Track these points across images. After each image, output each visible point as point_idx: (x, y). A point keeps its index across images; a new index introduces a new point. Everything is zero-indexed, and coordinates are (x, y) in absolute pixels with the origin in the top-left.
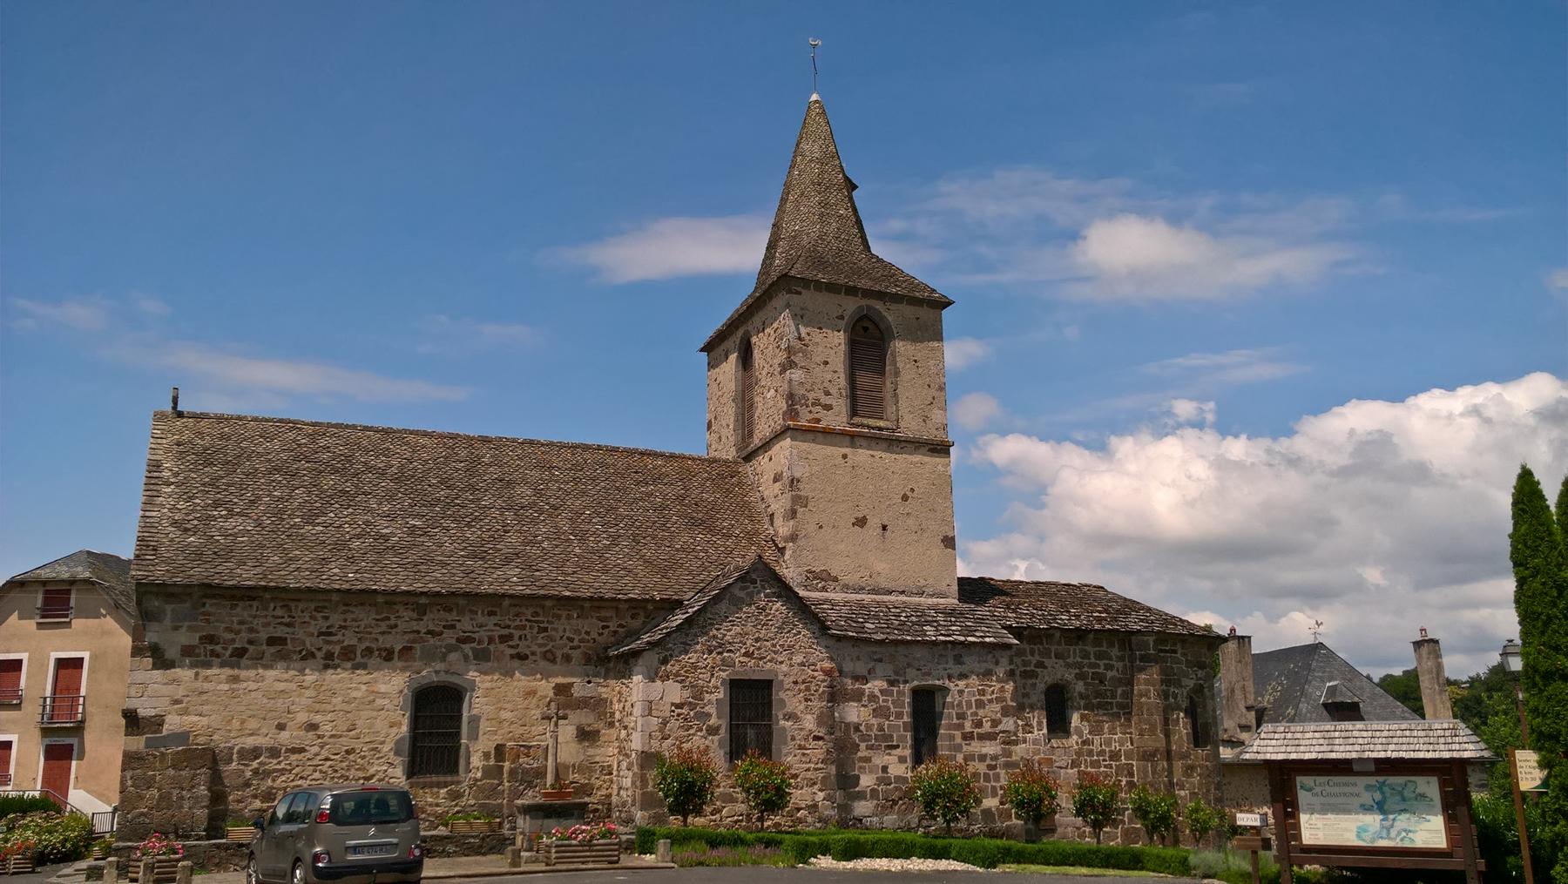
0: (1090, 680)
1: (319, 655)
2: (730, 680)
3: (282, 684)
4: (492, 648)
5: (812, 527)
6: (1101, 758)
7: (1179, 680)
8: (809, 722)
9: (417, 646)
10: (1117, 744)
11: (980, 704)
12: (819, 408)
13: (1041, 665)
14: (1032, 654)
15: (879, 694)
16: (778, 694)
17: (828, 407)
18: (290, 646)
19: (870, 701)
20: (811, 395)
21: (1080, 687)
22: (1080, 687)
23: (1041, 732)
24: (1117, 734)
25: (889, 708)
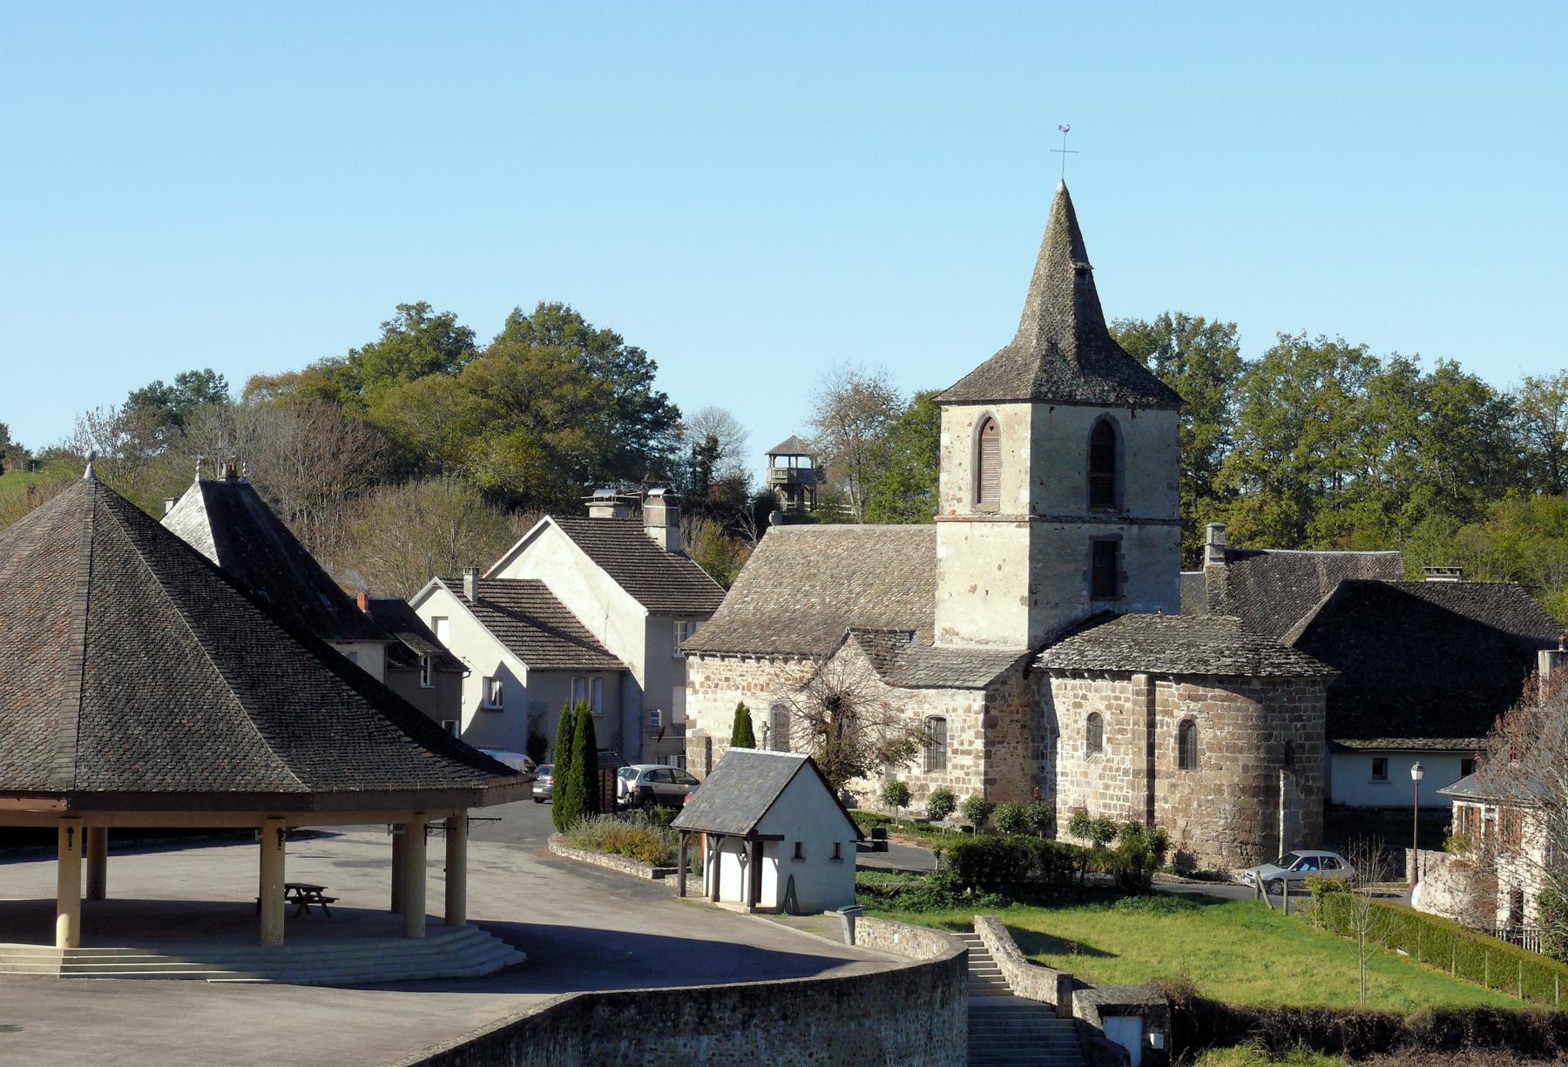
3: (1086, 526)
5: (946, 596)
11: (963, 730)
13: (1084, 697)
17: (960, 500)
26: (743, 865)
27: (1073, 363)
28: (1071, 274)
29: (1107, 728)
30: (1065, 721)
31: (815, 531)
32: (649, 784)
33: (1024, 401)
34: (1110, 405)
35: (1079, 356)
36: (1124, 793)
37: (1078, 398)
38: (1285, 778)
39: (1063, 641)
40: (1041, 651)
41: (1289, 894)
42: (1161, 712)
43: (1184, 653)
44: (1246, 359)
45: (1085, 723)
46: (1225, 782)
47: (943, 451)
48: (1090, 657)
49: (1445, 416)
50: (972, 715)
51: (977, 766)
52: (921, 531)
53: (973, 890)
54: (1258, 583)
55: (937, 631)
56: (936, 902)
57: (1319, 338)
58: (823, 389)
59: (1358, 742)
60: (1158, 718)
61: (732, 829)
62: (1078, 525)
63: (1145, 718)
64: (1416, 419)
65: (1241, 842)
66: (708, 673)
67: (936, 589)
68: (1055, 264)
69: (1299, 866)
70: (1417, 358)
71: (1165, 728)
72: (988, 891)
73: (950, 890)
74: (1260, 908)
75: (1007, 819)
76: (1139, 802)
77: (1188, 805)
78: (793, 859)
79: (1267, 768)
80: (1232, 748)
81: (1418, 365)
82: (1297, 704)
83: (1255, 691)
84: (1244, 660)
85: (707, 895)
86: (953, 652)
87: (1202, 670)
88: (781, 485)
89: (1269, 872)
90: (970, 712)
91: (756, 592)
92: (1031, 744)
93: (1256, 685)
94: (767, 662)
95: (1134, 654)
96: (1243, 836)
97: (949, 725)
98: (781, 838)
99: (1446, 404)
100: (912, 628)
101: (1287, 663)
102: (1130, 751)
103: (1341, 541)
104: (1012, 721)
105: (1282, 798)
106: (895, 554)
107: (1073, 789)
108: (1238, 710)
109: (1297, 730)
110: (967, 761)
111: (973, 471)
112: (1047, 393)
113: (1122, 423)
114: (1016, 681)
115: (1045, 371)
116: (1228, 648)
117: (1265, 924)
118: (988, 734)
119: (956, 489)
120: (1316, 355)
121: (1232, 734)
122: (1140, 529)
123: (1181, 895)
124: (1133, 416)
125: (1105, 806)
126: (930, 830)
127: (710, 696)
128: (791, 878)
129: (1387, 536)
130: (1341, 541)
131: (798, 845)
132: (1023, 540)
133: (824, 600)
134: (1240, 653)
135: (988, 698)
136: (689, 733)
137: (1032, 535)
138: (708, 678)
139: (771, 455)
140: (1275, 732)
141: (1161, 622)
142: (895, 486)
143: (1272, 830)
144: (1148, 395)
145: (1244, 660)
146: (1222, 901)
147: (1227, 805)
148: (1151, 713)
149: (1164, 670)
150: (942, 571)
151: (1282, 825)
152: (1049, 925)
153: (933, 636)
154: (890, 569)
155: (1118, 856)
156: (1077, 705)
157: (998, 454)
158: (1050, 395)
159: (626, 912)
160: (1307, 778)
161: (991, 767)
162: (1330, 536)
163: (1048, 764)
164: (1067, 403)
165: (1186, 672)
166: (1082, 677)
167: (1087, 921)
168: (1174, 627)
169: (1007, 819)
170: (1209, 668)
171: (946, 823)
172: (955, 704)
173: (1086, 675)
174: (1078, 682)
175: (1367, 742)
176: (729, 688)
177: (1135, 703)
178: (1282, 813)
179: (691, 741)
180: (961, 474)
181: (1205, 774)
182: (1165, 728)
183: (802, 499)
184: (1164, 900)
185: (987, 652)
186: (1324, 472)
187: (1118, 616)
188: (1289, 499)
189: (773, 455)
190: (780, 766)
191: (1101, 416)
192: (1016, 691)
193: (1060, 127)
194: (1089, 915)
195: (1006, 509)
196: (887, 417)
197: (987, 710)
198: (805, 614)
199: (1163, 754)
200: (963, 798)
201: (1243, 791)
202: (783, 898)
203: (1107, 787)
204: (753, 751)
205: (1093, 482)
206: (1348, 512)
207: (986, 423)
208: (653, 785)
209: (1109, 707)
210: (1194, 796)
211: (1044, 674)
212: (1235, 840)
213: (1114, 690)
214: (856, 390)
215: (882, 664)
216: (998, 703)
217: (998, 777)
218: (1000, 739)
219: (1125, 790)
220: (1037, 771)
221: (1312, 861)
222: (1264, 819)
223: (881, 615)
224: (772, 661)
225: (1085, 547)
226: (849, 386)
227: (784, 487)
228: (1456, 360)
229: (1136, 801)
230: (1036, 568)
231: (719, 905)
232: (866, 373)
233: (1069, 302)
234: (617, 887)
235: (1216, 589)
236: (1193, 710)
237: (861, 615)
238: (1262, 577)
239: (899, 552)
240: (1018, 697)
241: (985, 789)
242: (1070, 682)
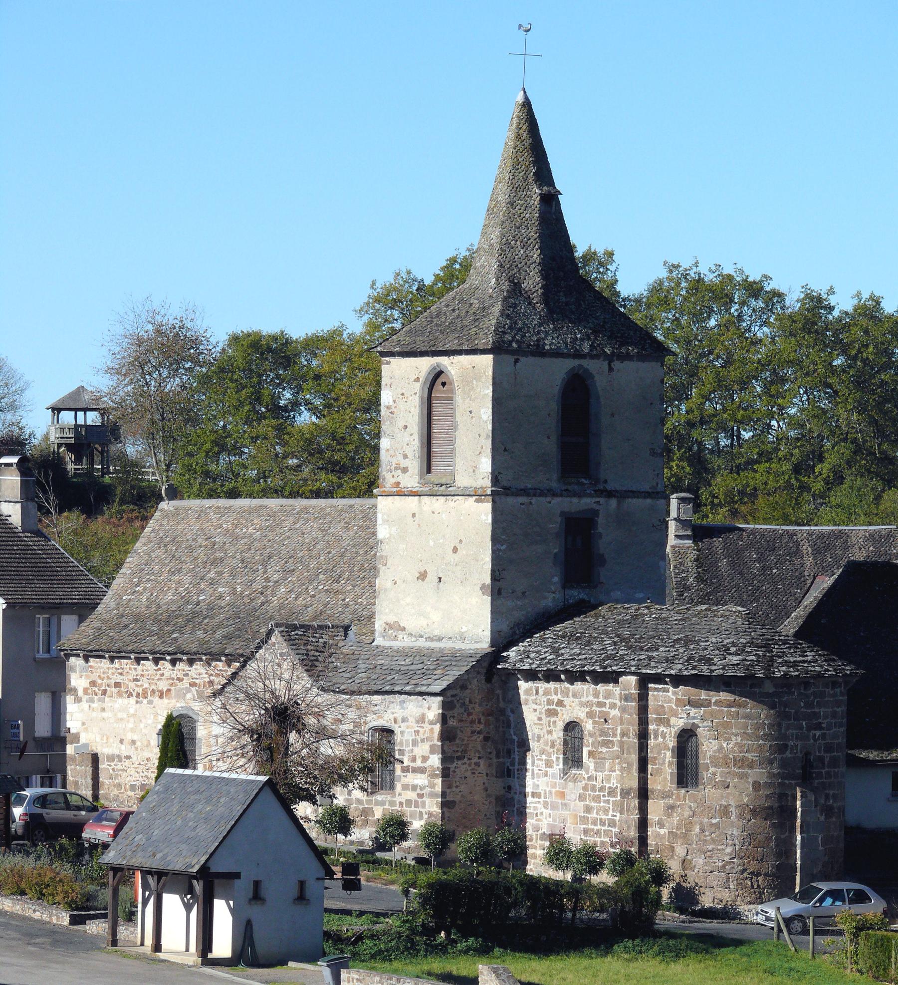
1: (134, 694)
5: (389, 584)
6: (602, 794)
7: (668, 720)
10: (615, 781)
11: (415, 743)
13: (560, 703)
17: (405, 470)
18: (122, 689)
23: (558, 767)
26: (188, 908)
27: (540, 307)
28: (536, 201)
29: (588, 740)
30: (536, 731)
31: (218, 507)
32: (39, 811)
33: (484, 352)
34: (583, 356)
35: (547, 297)
36: (610, 817)
37: (547, 347)
38: (802, 797)
39: (532, 637)
40: (507, 648)
41: (816, 933)
42: (656, 719)
43: (681, 650)
44: (624, 293)
45: (561, 734)
46: (732, 803)
47: (383, 411)
48: (567, 656)
49: (865, 361)
50: (426, 725)
51: (432, 786)
52: (351, 506)
53: (448, 934)
54: (732, 565)
55: (379, 626)
56: (407, 949)
57: (713, 268)
58: (119, 330)
59: (875, 753)
60: (652, 727)
61: (178, 865)
62: (548, 499)
63: (636, 727)
64: (830, 364)
65: (752, 873)
66: (94, 677)
67: (376, 577)
68: (517, 189)
69: (822, 900)
70: (831, 291)
71: (660, 739)
72: (465, 936)
73: (421, 934)
74: (782, 951)
75: (474, 850)
76: (629, 827)
77: (689, 831)
78: (250, 900)
79: (781, 785)
80: (740, 762)
81: (833, 300)
82: (817, 710)
83: (768, 695)
84: (754, 658)
85: (142, 944)
86: (398, 651)
87: (705, 670)
88: (67, 445)
89: (789, 907)
90: (424, 722)
91: (149, 580)
92: (495, 760)
93: (769, 688)
94: (167, 665)
95: (621, 652)
96: (754, 866)
97: (398, 738)
98: (237, 875)
99: (867, 346)
100: (347, 622)
101: (804, 662)
102: (617, 767)
103: (744, 509)
104: (473, 732)
105: (799, 821)
106: (320, 534)
107: (546, 812)
108: (747, 717)
109: (815, 740)
110: (421, 780)
111: (421, 436)
112: (511, 342)
113: (597, 378)
114: (477, 684)
115: (508, 316)
116: (734, 644)
117: (791, 969)
118: (445, 748)
119: (400, 458)
120: (711, 289)
121: (740, 746)
122: (619, 503)
123: (690, 937)
124: (611, 369)
125: (586, 832)
126: (377, 862)
127: (95, 705)
128: (249, 924)
129: (797, 504)
130: (744, 509)
131: (257, 884)
132: (483, 517)
133: (235, 589)
134: (748, 649)
135: (446, 706)
136: (70, 749)
137: (494, 510)
138: (93, 683)
139: (53, 409)
140: (791, 743)
141: (650, 614)
142: (208, 446)
143: (787, 857)
144: (628, 344)
145: (754, 658)
146: (737, 943)
147: (735, 830)
148: (643, 721)
149: (659, 671)
150: (383, 554)
151: (799, 852)
152: (543, 974)
153: (373, 632)
154: (314, 552)
155: (616, 892)
156: (551, 713)
157: (453, 415)
158: (515, 345)
159: (54, 965)
160: (827, 797)
161: (450, 787)
162: (729, 503)
163: (515, 783)
164: (533, 354)
165: (685, 673)
166: (558, 679)
167: (585, 968)
168: (665, 619)
169: (474, 850)
170: (713, 668)
171: (395, 854)
172: (406, 713)
173: (563, 677)
174: (552, 685)
175: (886, 753)
176: (120, 695)
177: (623, 710)
178: (799, 838)
179: (73, 759)
180: (407, 439)
181: (709, 793)
182: (660, 739)
183: (91, 462)
184: (671, 942)
185: (441, 650)
186: (723, 427)
187: (595, 607)
188: (680, 460)
189: (56, 410)
190: (233, 790)
191: (573, 368)
192: (478, 698)
193: (520, 26)
194: (585, 962)
195: (463, 480)
196: (196, 363)
197: (444, 719)
198: (211, 607)
199: (658, 769)
200: (417, 825)
201: (754, 812)
202: (239, 949)
203: (588, 809)
204: (188, 772)
205: (565, 447)
206: (751, 474)
207: (437, 377)
208: (44, 811)
209: (590, 715)
210: (695, 819)
211: (511, 676)
212: (744, 870)
213: (596, 695)
214: (159, 332)
215: (310, 665)
216: (458, 710)
217: (458, 798)
218: (459, 754)
219: (611, 813)
220: (503, 792)
221: (836, 895)
222: (777, 846)
223: (306, 607)
224: (173, 662)
225: (555, 525)
226: (150, 327)
227: (69, 447)
228: (877, 294)
229: (625, 827)
230: (500, 550)
231: (161, 955)
232: (170, 311)
233: (533, 234)
234: (31, 935)
235: (683, 571)
236: (694, 718)
237: (281, 607)
238: (736, 556)
239: (324, 531)
240: (480, 705)
241: (443, 813)
242: (542, 686)
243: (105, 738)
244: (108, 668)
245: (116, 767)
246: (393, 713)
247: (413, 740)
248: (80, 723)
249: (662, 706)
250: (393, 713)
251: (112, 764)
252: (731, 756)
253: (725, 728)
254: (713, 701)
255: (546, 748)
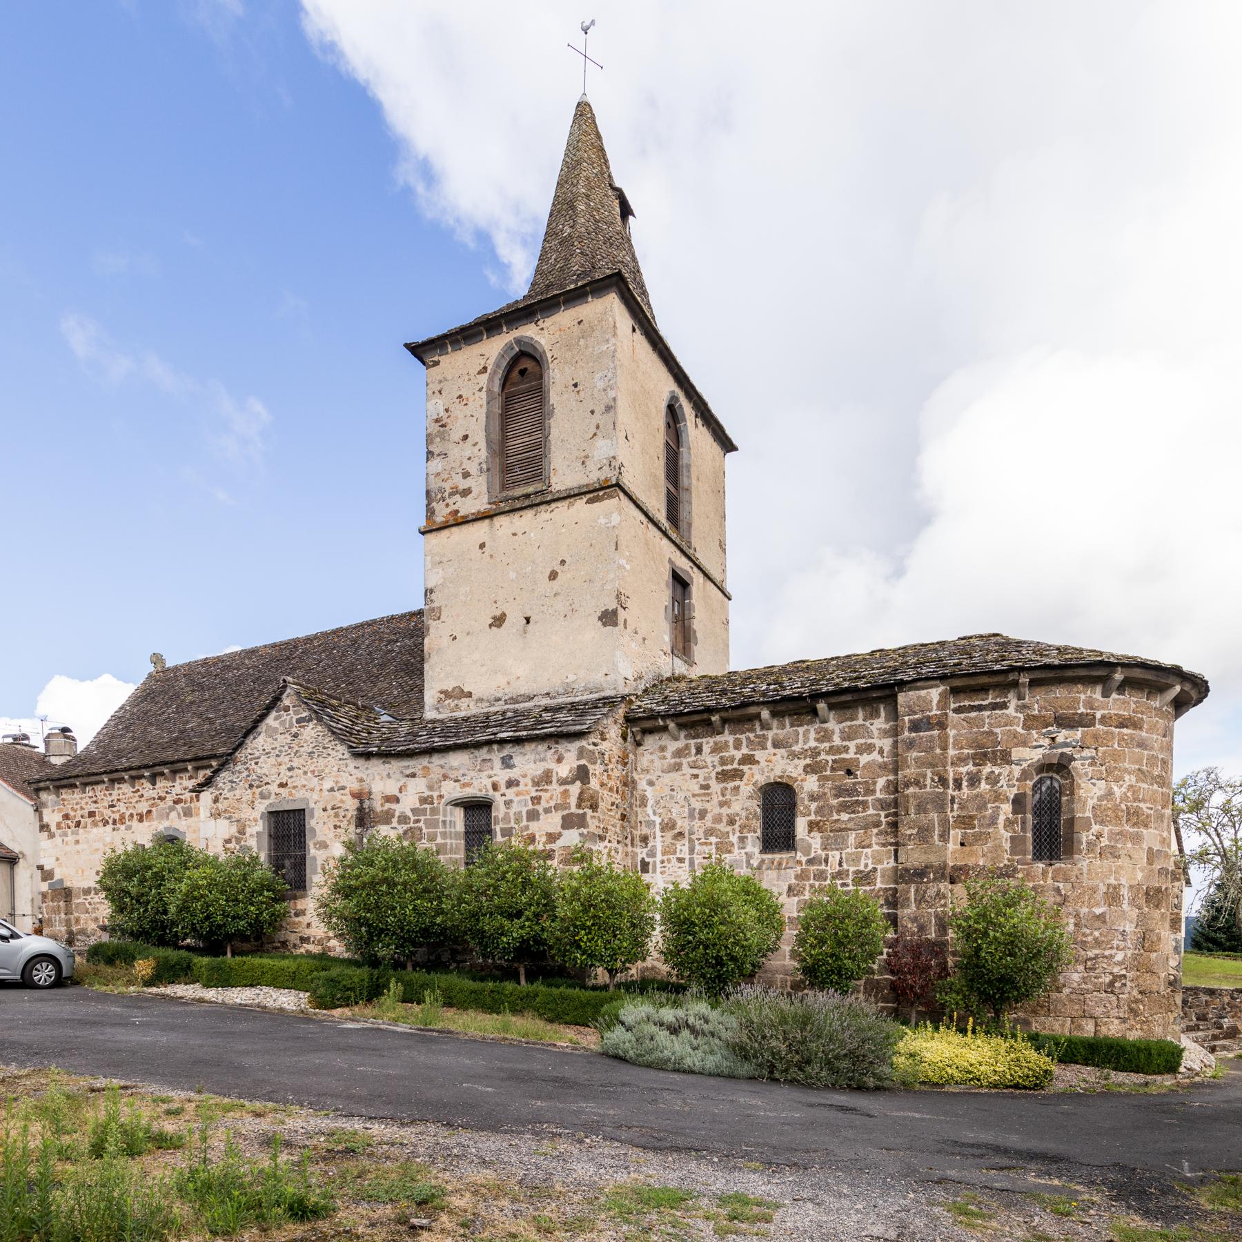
0: (828, 773)
1: (111, 821)
2: (269, 812)
4: (192, 805)
5: (446, 640)
6: (839, 882)
8: (338, 850)
9: (154, 809)
10: (870, 862)
11: (533, 816)
12: (457, 497)
14: (737, 746)
15: (410, 814)
16: (311, 823)
17: (466, 493)
18: (97, 818)
19: (399, 822)
20: (448, 486)
21: (811, 784)
22: (811, 784)
23: (743, 851)
24: (869, 846)
25: (420, 829)
46: (1123, 881)
87: (1038, 701)
94: (147, 785)
127: (70, 838)
138: (66, 817)
176: (95, 824)
236: (1066, 745)
243: (80, 871)
244: (81, 798)
245: (92, 901)
246: (490, 777)
247: (528, 812)
248: (54, 859)
249: (991, 733)
250: (490, 777)
251: (88, 897)
252: (1123, 807)
253: (1115, 761)
254: (1098, 716)
255: (718, 827)
